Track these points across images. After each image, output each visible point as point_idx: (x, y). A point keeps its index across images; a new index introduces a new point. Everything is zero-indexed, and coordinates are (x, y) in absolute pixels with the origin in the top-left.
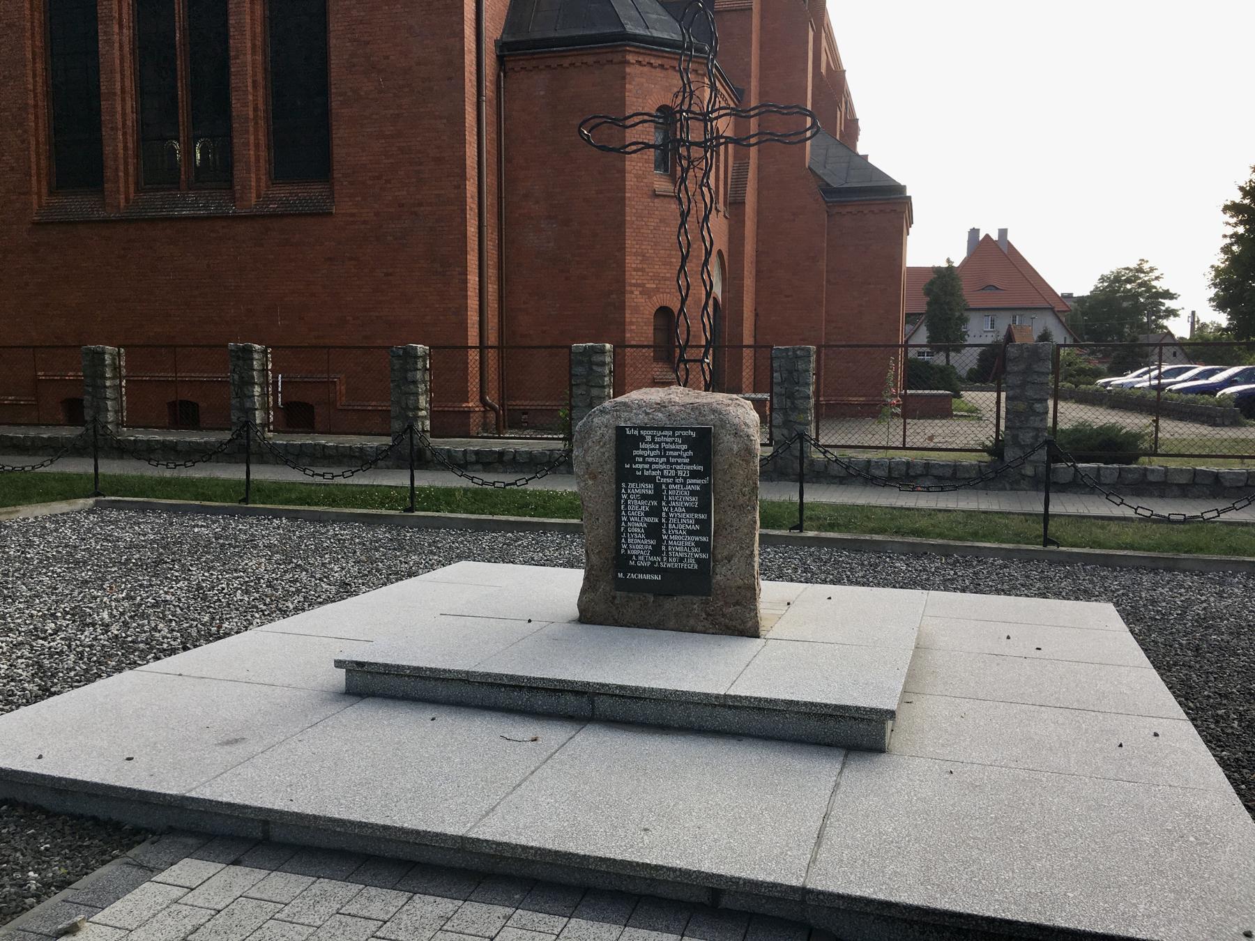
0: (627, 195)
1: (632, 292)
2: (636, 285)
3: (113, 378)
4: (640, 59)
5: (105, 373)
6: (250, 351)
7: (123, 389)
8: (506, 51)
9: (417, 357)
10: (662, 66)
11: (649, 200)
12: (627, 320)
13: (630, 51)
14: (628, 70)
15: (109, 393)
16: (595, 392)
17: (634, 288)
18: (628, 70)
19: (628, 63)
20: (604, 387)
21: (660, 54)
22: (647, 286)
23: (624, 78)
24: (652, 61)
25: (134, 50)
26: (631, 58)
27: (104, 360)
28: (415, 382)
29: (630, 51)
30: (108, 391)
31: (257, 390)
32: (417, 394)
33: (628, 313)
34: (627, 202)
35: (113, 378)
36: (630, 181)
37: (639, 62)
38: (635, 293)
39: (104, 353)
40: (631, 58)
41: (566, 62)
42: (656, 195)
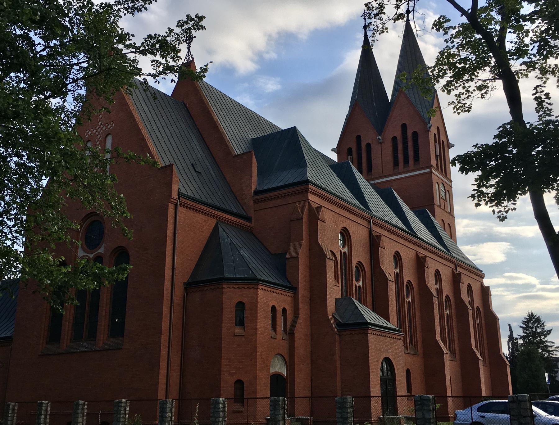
0: (223, 336)
1: (224, 374)
2: (226, 371)
3: (12, 413)
4: (229, 286)
5: (9, 411)
6: (42, 403)
7: (226, 408)
8: (189, 286)
9: (79, 405)
10: (238, 288)
11: (232, 338)
12: (222, 386)
13: (224, 284)
14: (224, 290)
15: (9, 418)
16: (119, 416)
17: (225, 373)
18: (224, 290)
19: (224, 288)
20: (121, 414)
21: (237, 283)
22: (231, 371)
23: (223, 293)
24: (235, 286)
25: (76, 293)
26: (225, 286)
27: (10, 407)
28: (78, 413)
29: (224, 284)
30: (10, 418)
31: (43, 417)
32: (78, 417)
33: (222, 382)
34: (223, 339)
35: (12, 413)
36: (224, 330)
37: (229, 287)
38: (226, 375)
39: (10, 405)
40: (225, 286)
41: (205, 289)
42: (236, 336)
